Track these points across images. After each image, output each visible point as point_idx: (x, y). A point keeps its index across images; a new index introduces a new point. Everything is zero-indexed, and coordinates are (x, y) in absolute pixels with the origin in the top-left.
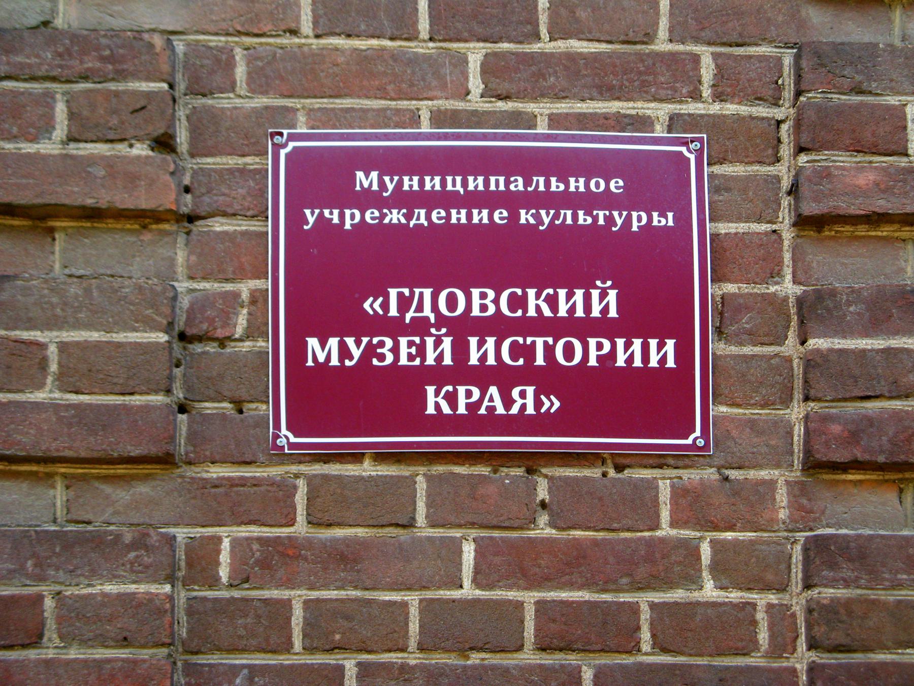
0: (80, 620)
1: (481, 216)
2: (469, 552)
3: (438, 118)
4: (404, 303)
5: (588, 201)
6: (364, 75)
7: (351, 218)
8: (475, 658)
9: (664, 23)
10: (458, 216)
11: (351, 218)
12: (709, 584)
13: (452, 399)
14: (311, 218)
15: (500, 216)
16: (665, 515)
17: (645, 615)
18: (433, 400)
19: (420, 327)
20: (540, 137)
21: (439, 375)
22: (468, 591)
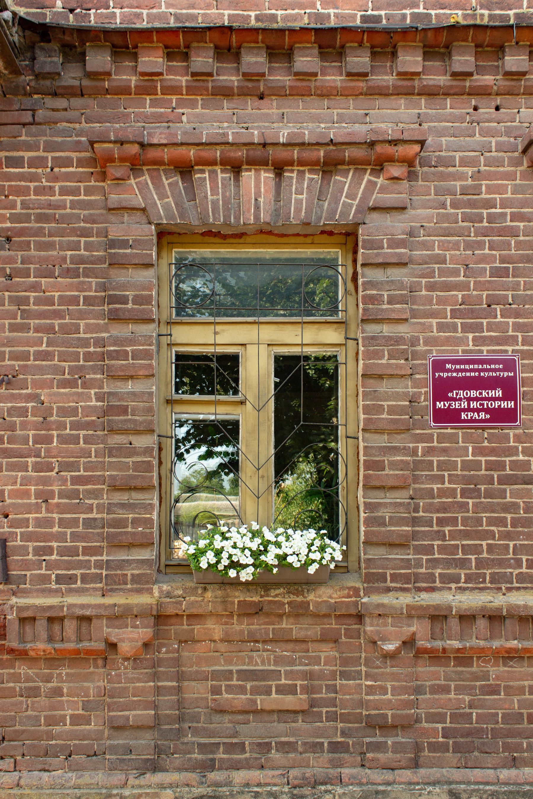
0: (393, 465)
1: (473, 374)
2: (470, 449)
3: (463, 351)
4: (457, 394)
5: (495, 370)
6: (447, 341)
7: (445, 375)
8: (472, 473)
9: (511, 328)
10: (468, 374)
11: (445, 375)
12: (521, 456)
13: (467, 415)
14: (437, 375)
15: (477, 374)
16: (512, 440)
17: (508, 463)
18: (463, 416)
19: (460, 400)
20: (485, 355)
21: (464, 410)
22: (470, 458)
